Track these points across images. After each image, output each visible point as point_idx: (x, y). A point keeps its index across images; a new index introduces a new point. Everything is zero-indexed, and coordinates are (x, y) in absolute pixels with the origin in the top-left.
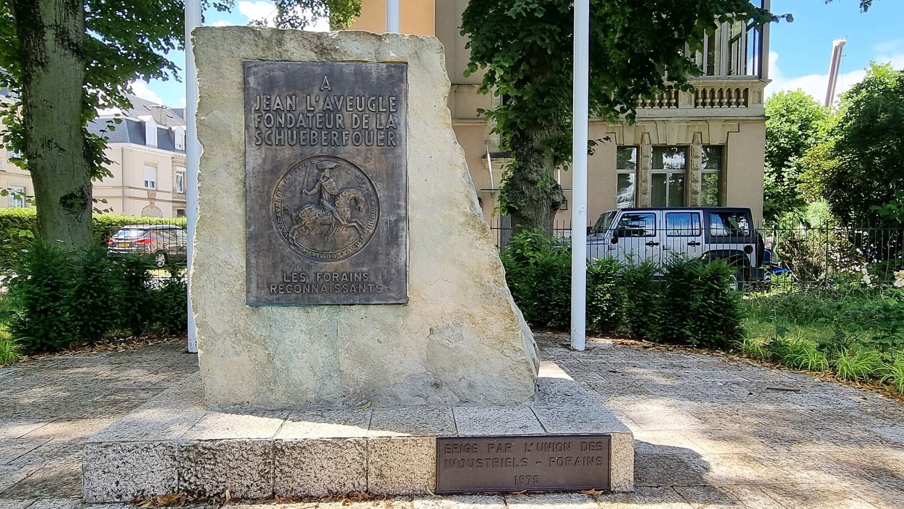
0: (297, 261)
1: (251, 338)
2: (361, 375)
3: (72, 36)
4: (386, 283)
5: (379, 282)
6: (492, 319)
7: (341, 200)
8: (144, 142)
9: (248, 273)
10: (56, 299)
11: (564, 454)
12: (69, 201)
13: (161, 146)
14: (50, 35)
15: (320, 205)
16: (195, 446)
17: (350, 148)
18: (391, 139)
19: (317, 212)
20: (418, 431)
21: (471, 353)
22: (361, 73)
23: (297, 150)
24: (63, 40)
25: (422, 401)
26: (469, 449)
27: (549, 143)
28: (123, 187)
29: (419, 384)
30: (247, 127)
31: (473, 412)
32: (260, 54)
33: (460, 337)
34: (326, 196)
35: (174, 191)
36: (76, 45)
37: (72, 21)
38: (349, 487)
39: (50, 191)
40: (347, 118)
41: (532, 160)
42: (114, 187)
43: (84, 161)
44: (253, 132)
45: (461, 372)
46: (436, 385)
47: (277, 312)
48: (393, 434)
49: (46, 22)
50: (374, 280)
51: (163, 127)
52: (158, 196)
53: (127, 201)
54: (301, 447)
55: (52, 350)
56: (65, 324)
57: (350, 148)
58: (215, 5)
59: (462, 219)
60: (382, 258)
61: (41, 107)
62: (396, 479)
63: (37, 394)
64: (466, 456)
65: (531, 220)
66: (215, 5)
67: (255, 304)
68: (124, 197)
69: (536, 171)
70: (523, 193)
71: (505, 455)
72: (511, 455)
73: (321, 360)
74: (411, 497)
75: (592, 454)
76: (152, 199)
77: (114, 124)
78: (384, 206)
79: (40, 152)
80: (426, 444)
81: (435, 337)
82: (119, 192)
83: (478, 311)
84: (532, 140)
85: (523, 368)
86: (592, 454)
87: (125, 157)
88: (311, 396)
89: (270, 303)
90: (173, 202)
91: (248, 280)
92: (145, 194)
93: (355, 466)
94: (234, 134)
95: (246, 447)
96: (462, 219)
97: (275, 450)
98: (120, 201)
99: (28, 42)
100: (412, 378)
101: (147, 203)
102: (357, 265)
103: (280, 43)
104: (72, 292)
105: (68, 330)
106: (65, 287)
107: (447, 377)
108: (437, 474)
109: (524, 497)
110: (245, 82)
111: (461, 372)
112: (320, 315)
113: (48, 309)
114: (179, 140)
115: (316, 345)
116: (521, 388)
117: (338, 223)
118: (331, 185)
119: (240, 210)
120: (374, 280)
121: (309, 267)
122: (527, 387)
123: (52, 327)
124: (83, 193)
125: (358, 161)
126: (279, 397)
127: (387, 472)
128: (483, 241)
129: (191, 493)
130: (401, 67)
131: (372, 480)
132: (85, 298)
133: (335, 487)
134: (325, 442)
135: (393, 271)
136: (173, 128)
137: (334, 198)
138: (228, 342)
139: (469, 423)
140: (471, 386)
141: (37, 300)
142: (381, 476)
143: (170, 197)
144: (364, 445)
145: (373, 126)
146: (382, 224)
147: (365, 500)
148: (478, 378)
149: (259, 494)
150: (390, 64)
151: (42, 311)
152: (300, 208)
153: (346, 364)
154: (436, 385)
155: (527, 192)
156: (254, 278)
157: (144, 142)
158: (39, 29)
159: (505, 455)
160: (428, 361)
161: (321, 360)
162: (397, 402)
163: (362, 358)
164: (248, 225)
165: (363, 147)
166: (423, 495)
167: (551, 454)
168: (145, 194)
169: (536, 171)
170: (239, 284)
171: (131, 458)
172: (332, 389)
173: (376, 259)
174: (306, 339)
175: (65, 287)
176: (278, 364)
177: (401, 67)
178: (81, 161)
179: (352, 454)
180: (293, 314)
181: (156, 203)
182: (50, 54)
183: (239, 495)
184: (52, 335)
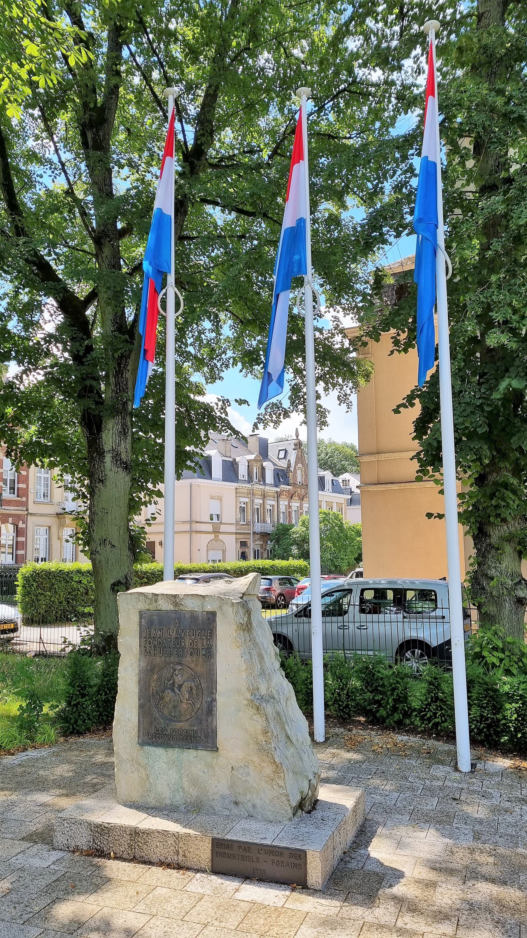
0: (162, 721)
1: (139, 764)
2: (193, 792)
3: (123, 456)
4: (206, 737)
5: (203, 737)
6: (265, 765)
7: (184, 688)
8: (210, 477)
9: (139, 726)
10: (83, 696)
11: (280, 859)
12: (116, 588)
13: (226, 478)
14: (108, 458)
15: (173, 690)
16: (101, 825)
17: (189, 658)
18: (209, 653)
19: (171, 694)
20: (204, 831)
21: (255, 785)
22: (193, 615)
23: (163, 658)
24: (117, 461)
25: (228, 813)
26: (228, 847)
27: (509, 539)
28: (191, 522)
29: (227, 801)
30: (140, 646)
31: (253, 825)
32: (147, 607)
33: (248, 774)
34: (176, 685)
35: (237, 524)
36: (126, 463)
37: (123, 445)
38: (169, 860)
39: (104, 580)
40: (187, 642)
41: (490, 556)
42: (183, 522)
43: (129, 553)
44: (143, 649)
45: (249, 797)
46: (236, 803)
47: (152, 749)
48: (191, 832)
49: (106, 449)
50: (200, 735)
51: (227, 459)
52: (223, 528)
53: (194, 535)
54: (148, 833)
55: (80, 734)
56: (88, 715)
57: (189, 658)
58: (236, 401)
59: (246, 702)
60: (204, 722)
61: (100, 514)
62: (192, 860)
63: (63, 770)
64: (227, 851)
65: (492, 616)
66: (236, 401)
67: (142, 744)
68: (191, 532)
69: (495, 567)
70: (483, 588)
71: (247, 854)
72: (250, 854)
73: (173, 780)
74: (198, 871)
75: (295, 861)
76: (216, 532)
77: (151, 522)
78: (205, 692)
79: (98, 549)
80: (207, 841)
81: (235, 773)
82: (187, 527)
83: (255, 759)
84: (490, 536)
85: (284, 799)
86: (295, 861)
87: (193, 492)
88: (168, 802)
89: (149, 744)
90: (236, 533)
91: (139, 730)
92: (209, 528)
93: (172, 848)
94: (134, 649)
95: (123, 829)
96: (246, 702)
97: (135, 833)
98: (187, 536)
99: (94, 465)
100: (223, 797)
101: (212, 536)
102: (191, 726)
103: (156, 601)
104: (95, 689)
105: (89, 719)
106: (91, 687)
107: (241, 799)
108: (212, 860)
109: (256, 882)
110: (140, 622)
111: (249, 797)
112: (174, 753)
113: (78, 703)
114: (243, 471)
115: (171, 771)
116: (283, 812)
117: (181, 701)
118: (179, 679)
119: (137, 690)
120: (200, 735)
121: (168, 725)
122: (286, 811)
123: (80, 716)
124: (127, 579)
125: (192, 666)
126: (152, 801)
127: (188, 855)
128: (258, 716)
129: (98, 851)
130: (213, 614)
131: (181, 858)
132: (101, 695)
133: (163, 859)
134: (158, 832)
135: (210, 731)
136: (238, 459)
137: (180, 686)
138: (128, 765)
139: (239, 832)
140: (254, 806)
141: (72, 698)
142: (184, 856)
143: (233, 529)
144: (177, 836)
145: (200, 647)
146: (204, 703)
147: (174, 868)
148: (258, 802)
149: (127, 857)
150: (208, 613)
151: (74, 705)
152: (163, 692)
153: (186, 784)
154: (236, 803)
155: (487, 588)
156: (141, 728)
157: (210, 477)
158: (101, 454)
159: (247, 854)
160: (232, 787)
161: (173, 780)
162: (212, 812)
163: (195, 782)
164: (139, 700)
165: (194, 658)
166: (204, 871)
167: (272, 857)
168: (209, 528)
169: (495, 567)
170: (135, 732)
171: (74, 827)
172: (179, 799)
173: (201, 723)
174: (170, 769)
175: (91, 687)
176: (152, 781)
177: (213, 614)
178: (126, 552)
179: (171, 841)
180: (159, 751)
181: (221, 537)
182: (108, 472)
183: (118, 855)
184: (80, 722)
